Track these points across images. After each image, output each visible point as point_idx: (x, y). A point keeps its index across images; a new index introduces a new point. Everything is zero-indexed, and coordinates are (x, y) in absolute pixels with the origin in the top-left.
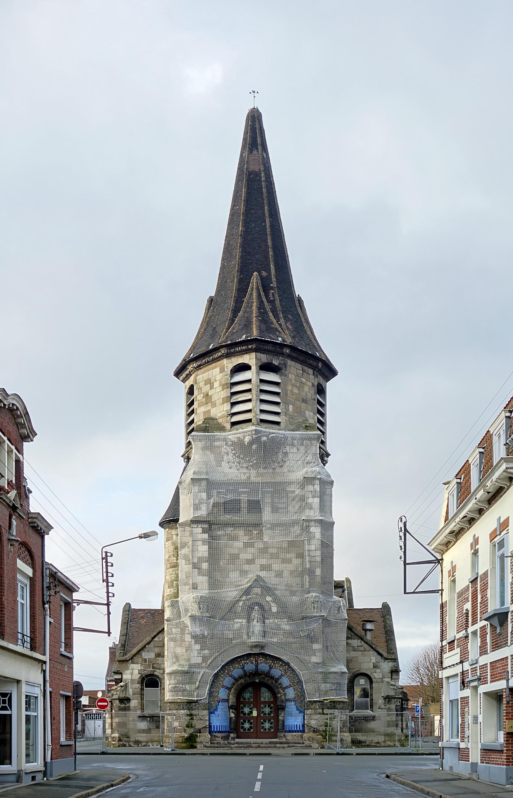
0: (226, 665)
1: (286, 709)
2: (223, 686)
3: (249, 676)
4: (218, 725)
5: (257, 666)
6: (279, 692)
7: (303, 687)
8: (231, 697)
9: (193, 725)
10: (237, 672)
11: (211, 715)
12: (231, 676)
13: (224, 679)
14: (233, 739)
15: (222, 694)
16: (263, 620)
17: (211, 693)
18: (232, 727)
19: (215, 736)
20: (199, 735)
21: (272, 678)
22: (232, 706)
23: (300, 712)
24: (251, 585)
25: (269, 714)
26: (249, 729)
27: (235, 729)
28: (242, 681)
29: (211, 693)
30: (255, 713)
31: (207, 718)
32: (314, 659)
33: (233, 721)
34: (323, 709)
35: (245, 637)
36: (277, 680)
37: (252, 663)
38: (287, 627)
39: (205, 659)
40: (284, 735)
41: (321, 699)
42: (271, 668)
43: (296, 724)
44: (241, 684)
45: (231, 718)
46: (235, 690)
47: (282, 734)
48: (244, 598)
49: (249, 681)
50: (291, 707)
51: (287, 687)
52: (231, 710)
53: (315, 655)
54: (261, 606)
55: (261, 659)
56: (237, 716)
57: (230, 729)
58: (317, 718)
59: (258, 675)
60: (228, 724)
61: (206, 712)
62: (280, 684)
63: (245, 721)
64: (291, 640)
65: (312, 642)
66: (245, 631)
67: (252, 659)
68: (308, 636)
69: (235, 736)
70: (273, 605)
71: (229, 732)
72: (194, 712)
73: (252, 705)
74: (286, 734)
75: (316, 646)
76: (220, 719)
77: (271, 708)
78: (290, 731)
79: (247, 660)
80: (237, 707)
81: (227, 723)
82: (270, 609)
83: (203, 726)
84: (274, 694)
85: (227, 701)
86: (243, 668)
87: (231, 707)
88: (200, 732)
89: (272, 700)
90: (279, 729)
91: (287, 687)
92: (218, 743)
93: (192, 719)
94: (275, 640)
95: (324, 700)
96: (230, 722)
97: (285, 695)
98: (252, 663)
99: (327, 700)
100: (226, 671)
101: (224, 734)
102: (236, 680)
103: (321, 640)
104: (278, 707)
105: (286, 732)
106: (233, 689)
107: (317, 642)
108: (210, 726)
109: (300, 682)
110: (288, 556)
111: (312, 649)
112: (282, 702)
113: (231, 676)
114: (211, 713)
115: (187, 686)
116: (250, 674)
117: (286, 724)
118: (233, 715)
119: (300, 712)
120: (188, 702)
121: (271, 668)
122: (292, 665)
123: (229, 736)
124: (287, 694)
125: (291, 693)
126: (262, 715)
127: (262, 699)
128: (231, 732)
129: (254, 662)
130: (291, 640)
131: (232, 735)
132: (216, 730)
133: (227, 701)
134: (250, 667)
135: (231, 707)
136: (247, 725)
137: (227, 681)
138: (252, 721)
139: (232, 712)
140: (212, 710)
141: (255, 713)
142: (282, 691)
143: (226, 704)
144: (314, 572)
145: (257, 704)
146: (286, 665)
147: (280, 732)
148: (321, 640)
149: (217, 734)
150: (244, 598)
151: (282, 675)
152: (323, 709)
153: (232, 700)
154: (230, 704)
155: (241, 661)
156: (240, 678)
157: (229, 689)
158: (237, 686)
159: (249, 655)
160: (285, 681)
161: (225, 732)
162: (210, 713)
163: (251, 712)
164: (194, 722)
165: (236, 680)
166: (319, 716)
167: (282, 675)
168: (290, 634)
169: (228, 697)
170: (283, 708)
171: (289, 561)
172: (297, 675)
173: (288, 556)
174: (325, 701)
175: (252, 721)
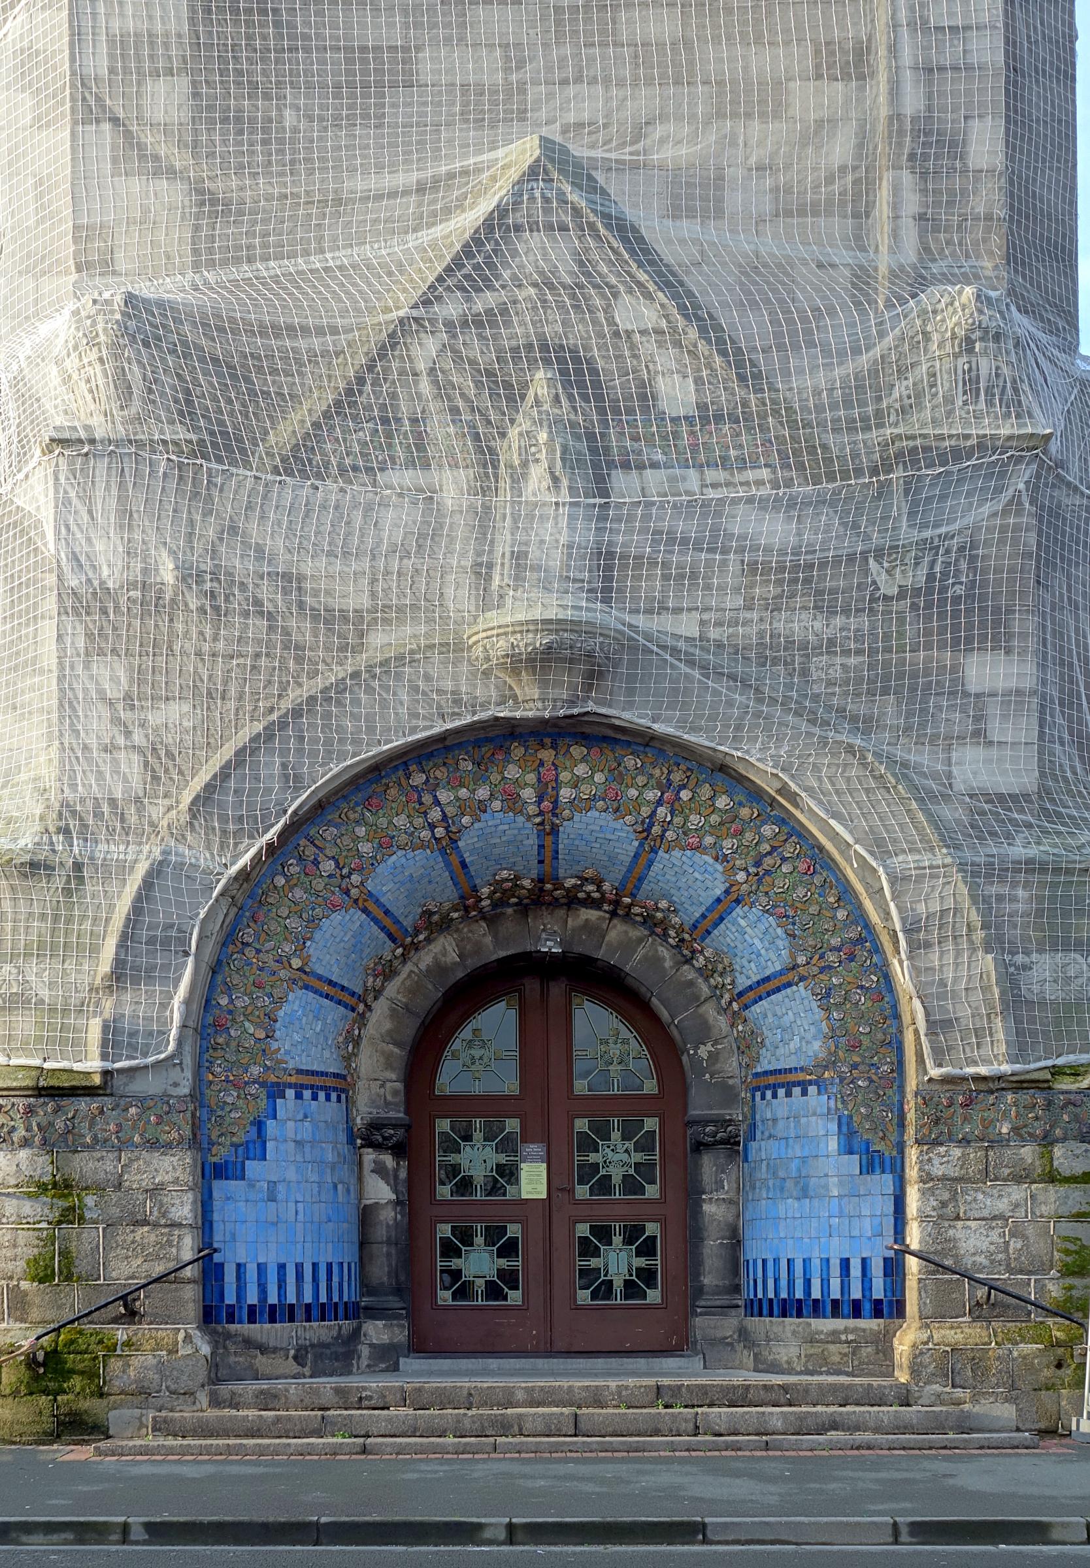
0: (319, 809)
1: (762, 1149)
2: (307, 980)
3: (492, 920)
4: (271, 1259)
5: (549, 831)
6: (704, 1032)
7: (887, 978)
8: (367, 1062)
9: (82, 1266)
10: (404, 876)
11: (220, 1188)
12: (367, 904)
13: (313, 923)
14: (387, 1359)
15: (304, 1034)
16: (594, 464)
17: (219, 1027)
18: (380, 1272)
19: (249, 1343)
20: (121, 1334)
21: (655, 924)
22: (375, 1125)
23: (868, 1168)
24: (501, 211)
25: (632, 1185)
26: (493, 1291)
27: (398, 1291)
28: (444, 950)
29: (208, 1023)
30: (533, 1181)
31: (183, 1209)
32: (974, 769)
33: (380, 1233)
34: (1047, 1142)
35: (458, 596)
36: (691, 939)
37: (513, 802)
38: (774, 532)
39: (159, 761)
40: (743, 1333)
41: (1035, 1066)
42: (650, 839)
43: (836, 1250)
44: (439, 970)
45: (366, 1215)
46: (394, 1014)
47: (727, 1326)
48: (452, 308)
49: (490, 945)
50: (805, 1133)
51: (768, 986)
52: (369, 1156)
53: (979, 735)
54: (576, 373)
55: (581, 772)
56: (414, 1198)
57: (367, 1287)
58: (1002, 1206)
59: (555, 904)
60: (348, 1254)
61: (172, 1168)
62: (706, 973)
63: (466, 1237)
64: (803, 624)
65: (963, 643)
66: (458, 557)
67: (512, 772)
68: (928, 597)
69: (400, 1335)
70: (665, 359)
71: (353, 1311)
72: (88, 1166)
73: (512, 1125)
74: (759, 1325)
75: (986, 672)
76: (295, 1210)
77: (645, 1146)
78: (791, 1308)
79: (480, 778)
80: (408, 1135)
81: (336, 1248)
82: (646, 397)
83: (159, 1269)
84: (664, 1045)
85: (338, 1086)
86: (448, 845)
87: (372, 1136)
88: (132, 1315)
89: (650, 1087)
90: (699, 1291)
91: (768, 986)
92: (266, 1401)
93: (71, 1216)
94: (687, 625)
95: (1057, 1071)
96: (364, 1243)
97: (749, 1044)
98: (513, 802)
99: (1076, 1072)
100: (328, 866)
101: (320, 1331)
102: (405, 940)
103: (1024, 623)
104: (698, 1135)
105: (757, 1308)
106: (381, 1008)
107: (998, 639)
108: (210, 1269)
109: (864, 943)
110: (762, 62)
111: (957, 690)
112: (729, 1095)
113: (367, 904)
114: (220, 1171)
115: (32, 969)
116: (504, 895)
117: (755, 1250)
118: (380, 1191)
119: (868, 1168)
120: (40, 1092)
121: (650, 839)
122: (812, 814)
123: (356, 1334)
124: (771, 1037)
125: (794, 1029)
126: (582, 1191)
127: (581, 1086)
128: (373, 1313)
129: (528, 794)
130: (803, 624)
131: (376, 1332)
132: (252, 1298)
133: (338, 1086)
134: (499, 837)
135: (372, 1136)
136: (479, 1263)
137: (338, 943)
138: (514, 1230)
139: (380, 1170)
140: (221, 1154)
141: (533, 1181)
142: (721, 1023)
143: (327, 1110)
144: (955, 147)
145: (541, 1104)
146: (763, 819)
147: (710, 1310)
148: (1024, 623)
149: (261, 1330)
150: (452, 308)
151: (731, 899)
152: (1047, 1142)
153: (377, 1086)
154: (364, 1111)
155: (432, 787)
156: (435, 924)
157: (355, 1003)
158: (414, 991)
159: (494, 739)
160: (754, 942)
161: (324, 1312)
162: (213, 1173)
163: (509, 1172)
164: (87, 1239)
165: (405, 940)
166: (1018, 1193)
167: (731, 899)
168: (799, 576)
169: (348, 1059)
170: (732, 1144)
171: (768, 101)
172: (846, 894)
173: (762, 62)
174: (1065, 1084)
175: (514, 1230)
